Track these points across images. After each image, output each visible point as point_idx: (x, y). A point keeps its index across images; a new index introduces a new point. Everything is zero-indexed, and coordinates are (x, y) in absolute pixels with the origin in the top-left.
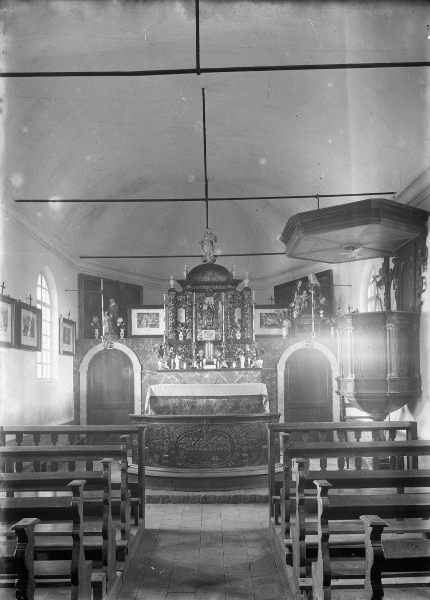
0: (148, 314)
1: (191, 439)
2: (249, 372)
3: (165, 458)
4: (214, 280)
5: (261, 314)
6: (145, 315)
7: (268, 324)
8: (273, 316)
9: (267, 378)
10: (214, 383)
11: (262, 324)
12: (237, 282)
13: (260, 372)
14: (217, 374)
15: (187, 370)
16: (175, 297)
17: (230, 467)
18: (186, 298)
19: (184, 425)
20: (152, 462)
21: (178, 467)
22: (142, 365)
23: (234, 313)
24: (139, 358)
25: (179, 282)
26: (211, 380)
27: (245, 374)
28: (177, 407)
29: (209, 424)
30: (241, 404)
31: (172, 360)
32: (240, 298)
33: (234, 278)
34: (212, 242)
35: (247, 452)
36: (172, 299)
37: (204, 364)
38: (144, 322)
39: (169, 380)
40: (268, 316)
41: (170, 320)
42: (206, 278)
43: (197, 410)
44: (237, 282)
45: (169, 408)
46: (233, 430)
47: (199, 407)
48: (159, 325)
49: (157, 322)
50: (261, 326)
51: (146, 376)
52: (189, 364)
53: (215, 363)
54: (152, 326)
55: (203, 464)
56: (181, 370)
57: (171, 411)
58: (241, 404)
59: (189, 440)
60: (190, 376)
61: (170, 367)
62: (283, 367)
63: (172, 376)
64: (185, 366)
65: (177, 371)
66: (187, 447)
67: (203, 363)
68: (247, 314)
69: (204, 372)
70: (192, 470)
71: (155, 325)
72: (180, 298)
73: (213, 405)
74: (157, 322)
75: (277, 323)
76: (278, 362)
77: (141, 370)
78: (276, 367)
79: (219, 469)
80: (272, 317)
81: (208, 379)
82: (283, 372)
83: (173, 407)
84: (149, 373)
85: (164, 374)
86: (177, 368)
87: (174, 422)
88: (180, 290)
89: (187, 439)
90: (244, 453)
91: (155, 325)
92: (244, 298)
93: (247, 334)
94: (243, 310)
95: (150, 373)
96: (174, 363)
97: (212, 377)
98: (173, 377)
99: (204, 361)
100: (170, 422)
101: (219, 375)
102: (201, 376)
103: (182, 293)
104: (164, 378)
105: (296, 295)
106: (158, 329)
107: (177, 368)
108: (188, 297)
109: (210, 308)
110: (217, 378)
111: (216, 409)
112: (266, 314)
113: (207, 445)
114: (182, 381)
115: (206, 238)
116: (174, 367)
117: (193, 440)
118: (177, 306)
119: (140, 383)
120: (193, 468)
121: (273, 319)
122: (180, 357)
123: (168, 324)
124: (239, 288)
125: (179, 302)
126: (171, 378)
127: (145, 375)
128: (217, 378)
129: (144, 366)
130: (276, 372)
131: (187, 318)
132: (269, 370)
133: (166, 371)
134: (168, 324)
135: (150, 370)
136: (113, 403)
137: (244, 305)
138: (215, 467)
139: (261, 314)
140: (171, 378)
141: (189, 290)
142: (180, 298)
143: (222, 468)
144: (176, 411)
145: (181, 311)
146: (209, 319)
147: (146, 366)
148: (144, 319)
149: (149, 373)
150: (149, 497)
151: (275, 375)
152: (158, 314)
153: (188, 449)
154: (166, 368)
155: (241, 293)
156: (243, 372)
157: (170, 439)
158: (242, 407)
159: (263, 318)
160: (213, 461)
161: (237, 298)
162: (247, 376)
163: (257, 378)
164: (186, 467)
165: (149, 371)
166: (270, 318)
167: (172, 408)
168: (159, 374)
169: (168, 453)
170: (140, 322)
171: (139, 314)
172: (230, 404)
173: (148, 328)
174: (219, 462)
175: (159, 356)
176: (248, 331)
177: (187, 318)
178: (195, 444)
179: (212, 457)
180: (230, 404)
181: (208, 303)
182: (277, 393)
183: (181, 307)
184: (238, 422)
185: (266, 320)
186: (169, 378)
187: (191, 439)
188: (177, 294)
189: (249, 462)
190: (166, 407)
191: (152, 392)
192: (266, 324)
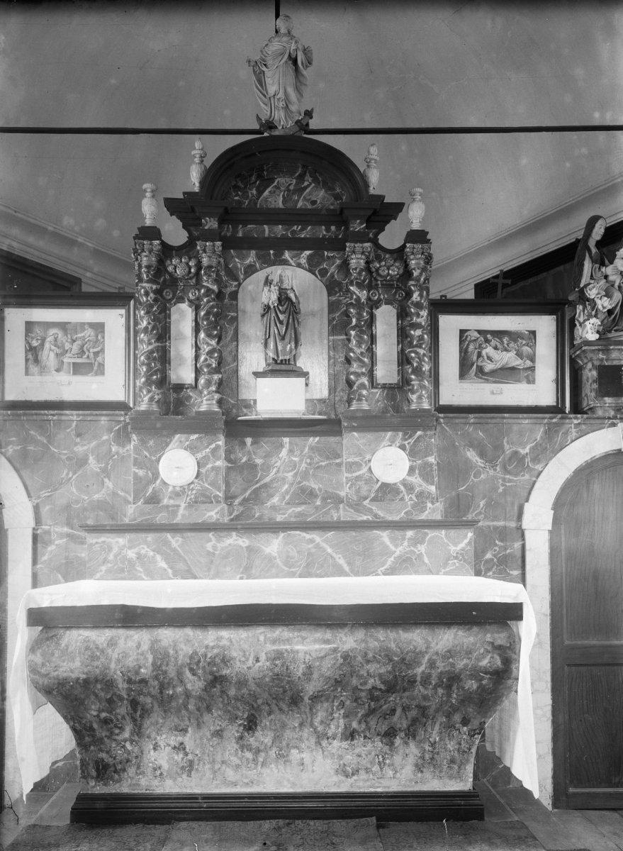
0: (63, 326)
2: (431, 534)
4: (300, 205)
5: (462, 332)
6: (52, 331)
7: (489, 367)
8: (505, 340)
9: (489, 556)
10: (300, 576)
11: (465, 367)
12: (383, 212)
13: (470, 535)
14: (312, 541)
16: (161, 262)
18: (199, 266)
22: (36, 509)
23: (372, 321)
24: (28, 483)
25: (173, 206)
26: (288, 562)
27: (416, 542)
28: (144, 681)
30: (419, 670)
32: (395, 271)
33: (372, 191)
34: (295, 61)
36: (148, 267)
38: (49, 356)
39: (130, 561)
40: (487, 341)
41: (142, 341)
42: (274, 198)
43: (232, 692)
44: (383, 212)
45: (109, 684)
47: (242, 683)
48: (101, 366)
49: (96, 354)
50: (463, 374)
51: (51, 548)
54: (78, 369)
57: (121, 698)
58: (419, 670)
62: (547, 517)
68: (417, 326)
69: (263, 536)
71: (88, 365)
72: (178, 267)
73: (300, 673)
74: (96, 354)
75: (517, 362)
76: (527, 500)
77: (32, 524)
80: (502, 343)
81: (278, 561)
82: (546, 536)
83: (130, 681)
84: (61, 536)
88: (175, 232)
91: (88, 365)
92: (407, 274)
93: (420, 397)
94: (403, 314)
95: (68, 535)
97: (294, 553)
98: (145, 550)
101: (318, 546)
102: (250, 549)
103: (187, 249)
105: (587, 265)
106: (99, 378)
108: (205, 261)
109: (289, 299)
110: (310, 554)
111: (310, 689)
112: (479, 332)
114: (181, 566)
115: (276, 46)
118: (168, 294)
119: (29, 573)
121: (506, 350)
123: (135, 357)
124: (391, 237)
125: (173, 282)
126: (139, 557)
127: (50, 542)
128: (310, 554)
129: (45, 510)
131: (202, 335)
132: (496, 528)
134: (135, 357)
135: (69, 524)
136: (580, 362)
137: (409, 294)
139: (462, 332)
140: (139, 557)
141: (210, 236)
142: (178, 267)
144: (141, 699)
145: (182, 313)
146: (283, 338)
148: (47, 345)
149: (61, 536)
151: (517, 545)
152: (99, 327)
155: (399, 254)
156: (410, 533)
158: (426, 680)
159: (471, 347)
161: (384, 272)
162: (422, 548)
163: (460, 556)
166: (496, 348)
167: (122, 685)
168: (92, 539)
170: (33, 353)
171: (29, 326)
172: (372, 668)
173: (63, 377)
176: (422, 387)
177: (202, 335)
180: (372, 668)
181: (281, 281)
183: (181, 300)
185: (479, 355)
186: (131, 554)
188: (167, 251)
190: (97, 681)
192: (480, 370)
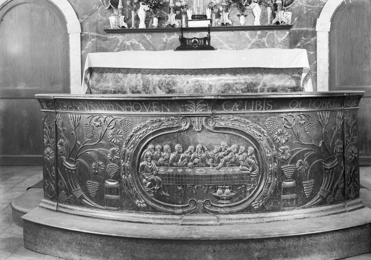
1: (166, 147)
3: (111, 190)
15: (159, 30)
17: (257, 211)
19: (152, 116)
20: (82, 197)
21: (138, 209)
27: (261, 37)
29: (209, 112)
31: (133, 12)
35: (294, 177)
37: (190, 18)
46: (265, 127)
52: (161, 19)
53: (209, 17)
55: (196, 204)
56: (149, 30)
59: (162, 150)
60: (164, 39)
61: (129, 25)
63: (134, 39)
64: (155, 22)
65: (142, 31)
66: (160, 165)
67: (187, 18)
70: (170, 216)
78: (314, 25)
79: (231, 216)
85: (120, 37)
86: (142, 25)
87: (129, 110)
89: (158, 146)
90: (286, 179)
96: (137, 18)
99: (190, 14)
100: (120, 110)
104: (119, 45)
107: (142, 25)
113: (203, 160)
116: (137, 25)
117: (173, 150)
120: (174, 214)
122: (147, 7)
129: (86, 24)
130: (314, 34)
133: (122, 31)
138: (222, 210)
143: (238, 212)
147: (90, 24)
150: (261, 20)
153: (162, 170)
154: (123, 27)
156: (259, 32)
157: (120, 146)
160: (218, 198)
162: (265, 39)
164: (155, 211)
165: (95, 34)
169: (117, 177)
174: (230, 199)
175: (110, 7)
178: (175, 160)
179: (215, 189)
182: (316, 70)
184: (273, 109)
187: (166, 147)
189: (297, 199)
191: (90, 63)
